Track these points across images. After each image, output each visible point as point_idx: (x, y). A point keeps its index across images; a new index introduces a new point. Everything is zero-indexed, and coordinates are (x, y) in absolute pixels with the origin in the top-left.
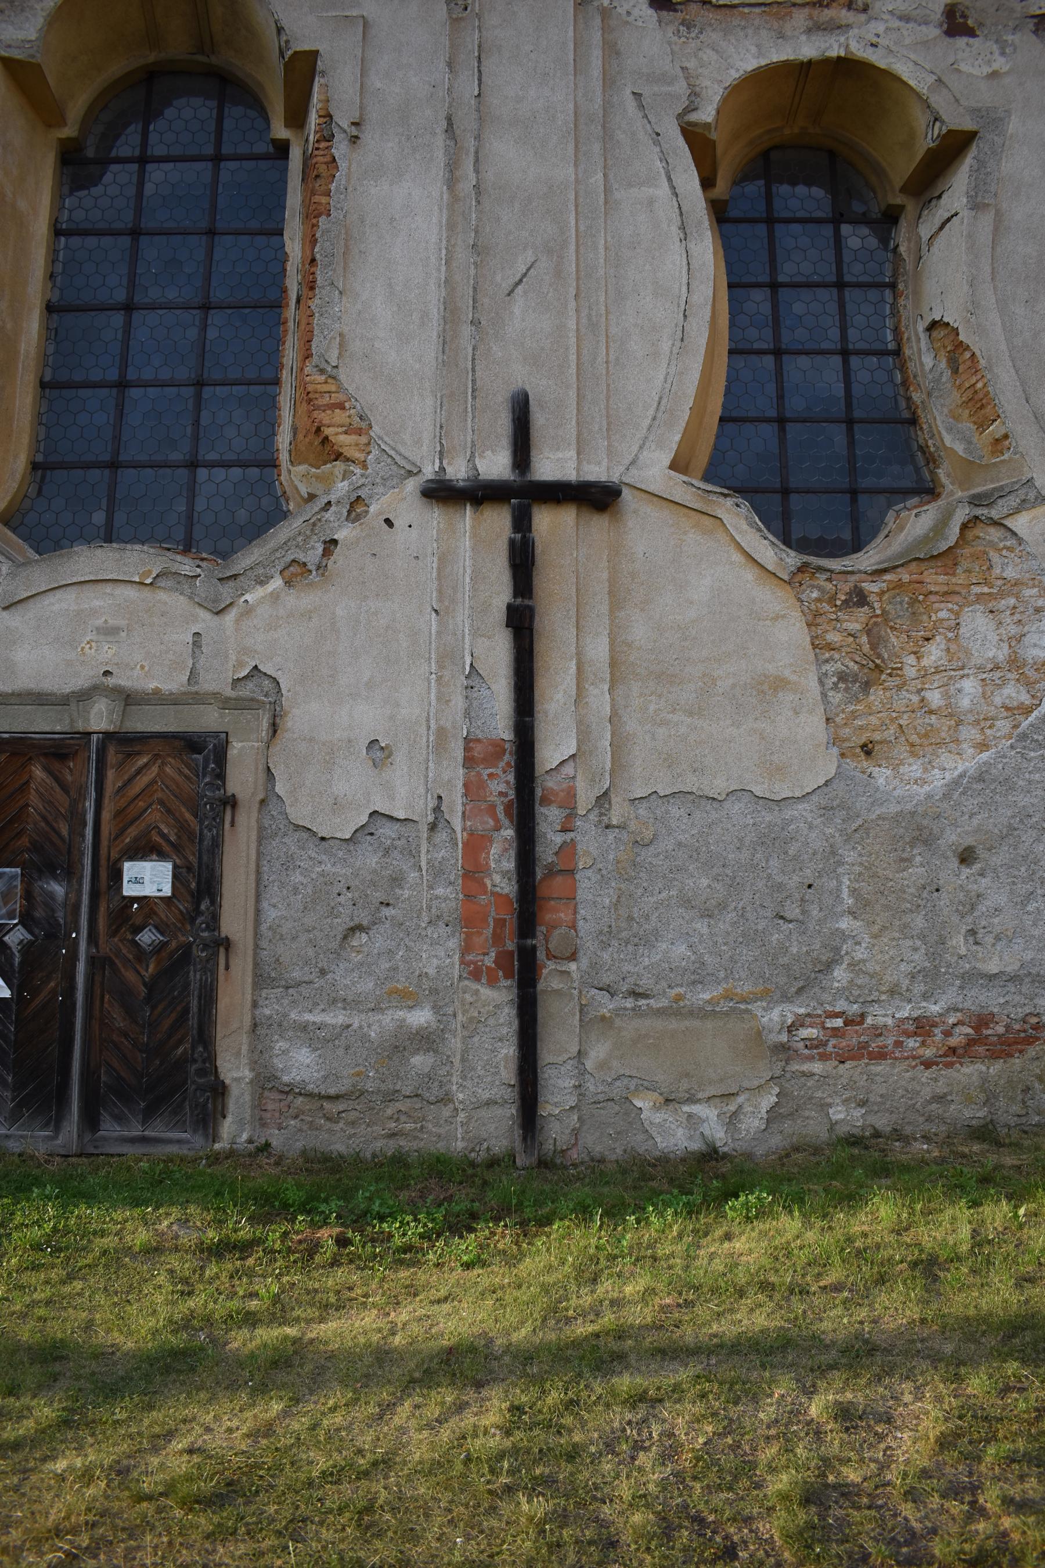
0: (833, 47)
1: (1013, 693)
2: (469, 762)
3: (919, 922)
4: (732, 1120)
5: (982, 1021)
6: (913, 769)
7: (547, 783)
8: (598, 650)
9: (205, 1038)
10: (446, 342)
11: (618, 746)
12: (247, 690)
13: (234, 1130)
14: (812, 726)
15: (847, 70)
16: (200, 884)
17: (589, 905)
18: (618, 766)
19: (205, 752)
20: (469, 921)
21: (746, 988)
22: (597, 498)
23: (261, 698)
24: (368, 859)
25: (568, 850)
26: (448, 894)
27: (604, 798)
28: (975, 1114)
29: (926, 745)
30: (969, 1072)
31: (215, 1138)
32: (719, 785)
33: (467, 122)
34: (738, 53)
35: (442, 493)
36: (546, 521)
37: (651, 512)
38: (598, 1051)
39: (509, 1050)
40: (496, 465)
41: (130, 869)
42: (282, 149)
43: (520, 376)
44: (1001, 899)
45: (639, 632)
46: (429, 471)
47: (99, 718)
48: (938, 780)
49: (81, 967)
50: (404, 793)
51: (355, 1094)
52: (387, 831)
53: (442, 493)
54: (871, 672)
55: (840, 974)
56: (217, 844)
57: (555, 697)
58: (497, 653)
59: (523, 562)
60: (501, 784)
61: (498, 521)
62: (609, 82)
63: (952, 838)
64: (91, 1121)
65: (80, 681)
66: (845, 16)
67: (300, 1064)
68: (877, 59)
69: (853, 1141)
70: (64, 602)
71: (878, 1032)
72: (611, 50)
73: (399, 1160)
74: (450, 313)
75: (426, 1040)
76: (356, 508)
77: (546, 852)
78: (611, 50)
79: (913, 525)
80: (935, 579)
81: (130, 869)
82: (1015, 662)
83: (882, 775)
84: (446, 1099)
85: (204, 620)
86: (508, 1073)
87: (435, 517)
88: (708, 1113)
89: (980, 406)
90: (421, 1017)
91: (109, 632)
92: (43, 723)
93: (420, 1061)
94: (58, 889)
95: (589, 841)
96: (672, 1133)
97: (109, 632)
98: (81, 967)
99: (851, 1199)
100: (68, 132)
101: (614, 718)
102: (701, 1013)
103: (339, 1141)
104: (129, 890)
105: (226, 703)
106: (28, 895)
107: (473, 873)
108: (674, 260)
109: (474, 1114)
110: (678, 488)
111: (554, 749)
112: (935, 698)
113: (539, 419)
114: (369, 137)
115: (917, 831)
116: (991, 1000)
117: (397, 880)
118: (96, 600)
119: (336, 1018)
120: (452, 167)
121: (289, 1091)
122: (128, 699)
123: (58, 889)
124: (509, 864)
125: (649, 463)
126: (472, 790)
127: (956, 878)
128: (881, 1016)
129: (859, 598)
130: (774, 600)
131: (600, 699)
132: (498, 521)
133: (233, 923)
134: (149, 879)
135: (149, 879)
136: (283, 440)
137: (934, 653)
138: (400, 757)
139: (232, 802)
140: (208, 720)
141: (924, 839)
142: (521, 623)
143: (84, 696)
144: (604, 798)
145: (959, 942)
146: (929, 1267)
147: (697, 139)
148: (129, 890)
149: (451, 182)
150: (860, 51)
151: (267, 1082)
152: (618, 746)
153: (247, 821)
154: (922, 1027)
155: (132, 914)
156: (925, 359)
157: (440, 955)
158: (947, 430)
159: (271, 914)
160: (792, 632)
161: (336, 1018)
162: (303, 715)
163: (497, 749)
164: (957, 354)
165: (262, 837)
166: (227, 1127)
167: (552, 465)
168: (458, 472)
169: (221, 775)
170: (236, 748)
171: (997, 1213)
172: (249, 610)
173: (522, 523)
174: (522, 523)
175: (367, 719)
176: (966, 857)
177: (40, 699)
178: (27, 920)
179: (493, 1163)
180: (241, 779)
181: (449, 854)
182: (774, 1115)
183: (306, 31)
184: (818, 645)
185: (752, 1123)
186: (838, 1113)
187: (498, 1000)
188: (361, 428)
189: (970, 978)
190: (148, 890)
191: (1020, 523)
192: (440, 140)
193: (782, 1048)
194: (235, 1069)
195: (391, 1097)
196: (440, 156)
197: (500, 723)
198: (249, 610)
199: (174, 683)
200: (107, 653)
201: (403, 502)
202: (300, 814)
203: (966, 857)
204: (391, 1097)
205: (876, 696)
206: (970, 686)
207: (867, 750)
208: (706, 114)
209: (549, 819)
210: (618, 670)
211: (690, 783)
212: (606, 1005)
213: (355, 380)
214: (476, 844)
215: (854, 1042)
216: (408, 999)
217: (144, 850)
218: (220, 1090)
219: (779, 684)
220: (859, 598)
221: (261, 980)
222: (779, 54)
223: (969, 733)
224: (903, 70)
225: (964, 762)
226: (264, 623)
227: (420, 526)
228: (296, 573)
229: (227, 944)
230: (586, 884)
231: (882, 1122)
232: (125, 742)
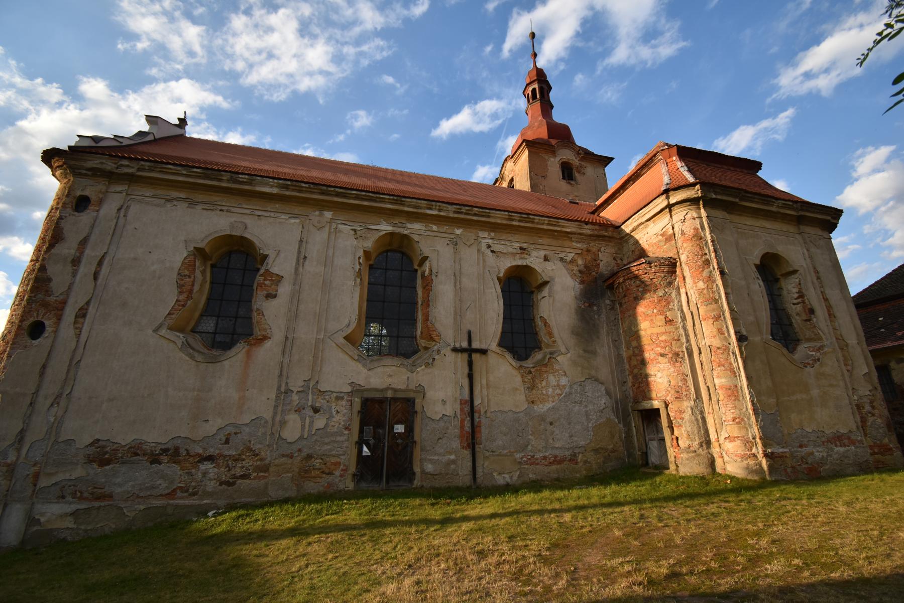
0: (524, 263)
1: (558, 391)
2: (461, 404)
3: (543, 437)
4: (511, 478)
5: (556, 457)
6: (541, 406)
7: (476, 409)
8: (484, 382)
9: (411, 463)
10: (455, 319)
11: (488, 401)
12: (418, 389)
13: (417, 483)
14: (523, 398)
15: (527, 267)
16: (410, 430)
17: (484, 433)
18: (488, 406)
19: (409, 403)
20: (461, 437)
21: (512, 450)
22: (484, 352)
23: (421, 390)
24: (442, 424)
25: (480, 422)
26: (457, 431)
27: (486, 412)
28: (555, 476)
29: (543, 401)
30: (554, 467)
31: (412, 484)
32: (506, 409)
33: (457, 274)
34: (507, 263)
35: (455, 350)
36: (474, 356)
37: (493, 355)
38: (486, 464)
39: (470, 464)
40: (465, 344)
41: (396, 426)
42: (416, 271)
43: (469, 327)
44: (557, 432)
45: (491, 378)
46: (452, 345)
47: (389, 394)
48: (545, 408)
49: (386, 449)
50: (449, 410)
51: (440, 474)
52: (445, 418)
53: (455, 350)
54: (532, 387)
55: (530, 447)
56: (413, 421)
57: (477, 392)
58: (466, 382)
59: (470, 364)
60: (467, 409)
61: (466, 355)
62: (484, 268)
63: (548, 420)
64: (387, 482)
65: (384, 387)
66: (526, 256)
67: (429, 468)
68: (531, 265)
69: (534, 481)
70: (380, 369)
71: (537, 459)
72: (484, 261)
73: (449, 487)
74: (456, 314)
75: (453, 462)
76: (439, 352)
77: (476, 423)
78: (484, 261)
79: (538, 356)
80: (544, 369)
81: (396, 426)
82: (558, 385)
83: (535, 407)
84: (458, 474)
85: (409, 374)
86: (470, 468)
87: (454, 354)
88: (507, 476)
89: (550, 334)
90: (453, 457)
91: (390, 376)
92: (378, 395)
93: (453, 466)
94: (381, 431)
95: (483, 420)
96: (500, 480)
97: (390, 376)
98: (386, 449)
99: (540, 491)
100: (371, 262)
101: (488, 396)
102: (505, 455)
103: (437, 485)
104: (396, 431)
105: (414, 392)
106: (374, 432)
107: (462, 427)
108: (496, 304)
109: (463, 476)
110: (498, 350)
111: (477, 402)
112: (544, 392)
113: (472, 335)
114: (439, 276)
115: (542, 418)
116: (557, 452)
117: (448, 428)
118: (387, 369)
119: (436, 458)
120: (455, 283)
121: (427, 474)
122: (395, 390)
123: (381, 431)
124: (469, 425)
125: (493, 345)
126: (462, 410)
127: (550, 428)
128: (538, 456)
129: (530, 372)
130: (515, 372)
131: (485, 392)
132: (466, 355)
133: (416, 438)
134: (400, 429)
135: (400, 429)
136: (419, 333)
137: (544, 383)
138: (448, 403)
139: (416, 412)
140: (412, 395)
141: (543, 420)
142: (471, 377)
143: (387, 389)
144: (486, 412)
145: (551, 441)
146: (559, 500)
147: (499, 279)
148: (396, 431)
149: (455, 286)
150: (529, 264)
151: (423, 472)
152: (488, 401)
153: (419, 416)
154: (545, 458)
155: (394, 436)
156: (540, 323)
157: (456, 444)
158: (545, 339)
159: (423, 436)
160: (519, 379)
161: (436, 458)
162: (430, 394)
163: (466, 402)
164: (546, 323)
165: (422, 419)
166: (415, 482)
167: (476, 345)
168: (458, 346)
169: (414, 407)
170: (417, 401)
171: (566, 492)
172: (418, 372)
173: (470, 356)
174: (470, 356)
175: (441, 395)
176: (551, 424)
177: (376, 390)
178: (374, 438)
179: (468, 488)
180: (418, 408)
181: (457, 423)
182: (519, 477)
183: (426, 252)
184: (524, 382)
185: (515, 478)
186: (531, 476)
187: (467, 453)
188: (439, 335)
189: (553, 448)
190: (399, 431)
191: (558, 358)
192: (453, 277)
193: (520, 463)
194: (417, 469)
195: (447, 474)
196: (453, 281)
197: (466, 396)
198: (418, 372)
199: (403, 387)
200: (390, 380)
201: (447, 351)
202: (429, 415)
203: (551, 424)
204: (447, 474)
205: (534, 391)
206: (550, 390)
207: (533, 402)
208: (501, 275)
209: (476, 415)
210: (488, 386)
211: (501, 409)
212: (488, 454)
213: (437, 325)
214: (462, 421)
215: (533, 461)
216: (450, 453)
217: (398, 423)
218: (414, 474)
219: (517, 389)
220: (530, 372)
221: (422, 450)
222: (514, 263)
223: (551, 399)
224: (537, 268)
225: (549, 405)
226: (422, 376)
227: (451, 357)
228: (427, 365)
229: (415, 442)
230: (483, 429)
231: (539, 478)
232: (394, 399)
